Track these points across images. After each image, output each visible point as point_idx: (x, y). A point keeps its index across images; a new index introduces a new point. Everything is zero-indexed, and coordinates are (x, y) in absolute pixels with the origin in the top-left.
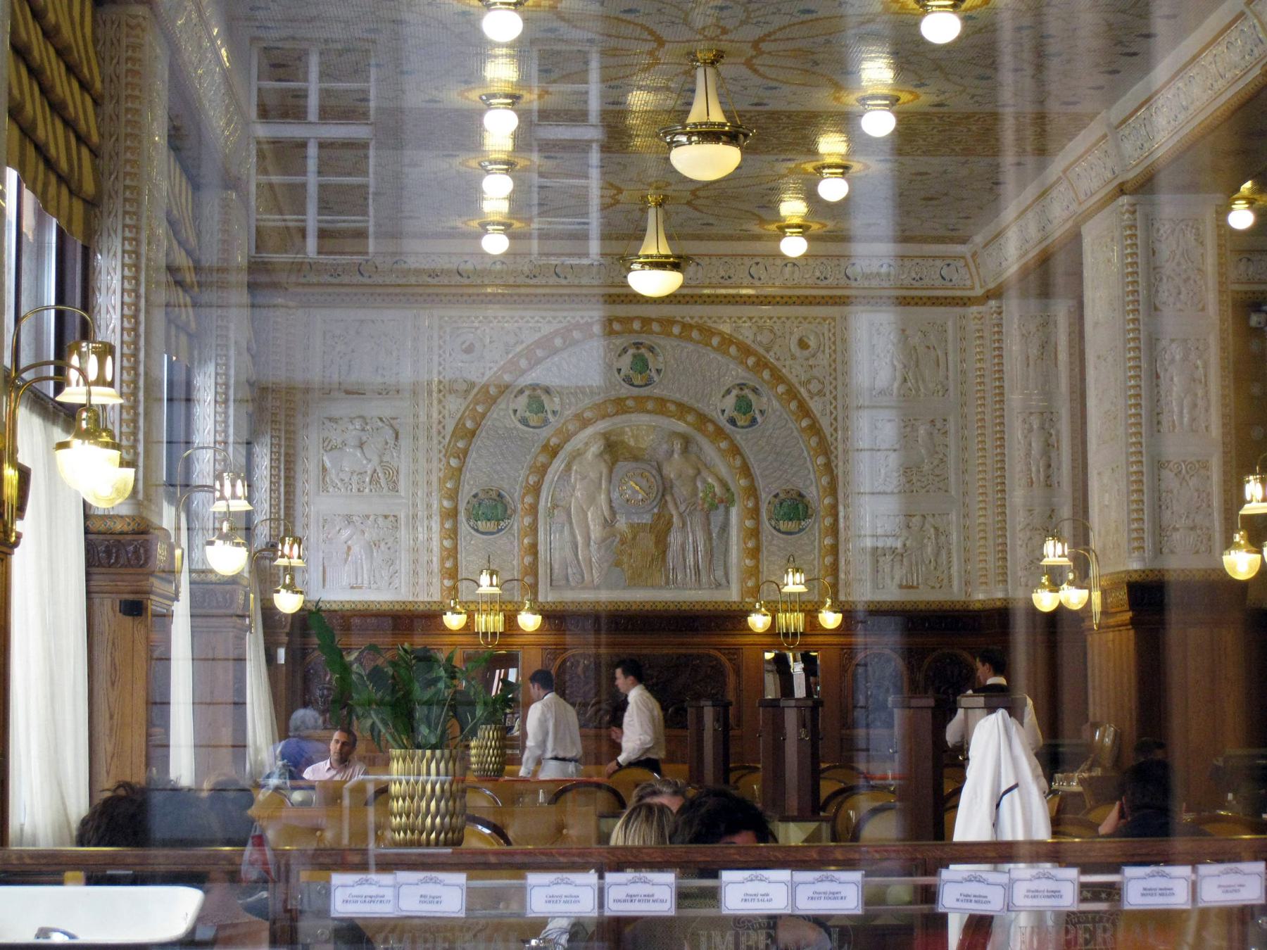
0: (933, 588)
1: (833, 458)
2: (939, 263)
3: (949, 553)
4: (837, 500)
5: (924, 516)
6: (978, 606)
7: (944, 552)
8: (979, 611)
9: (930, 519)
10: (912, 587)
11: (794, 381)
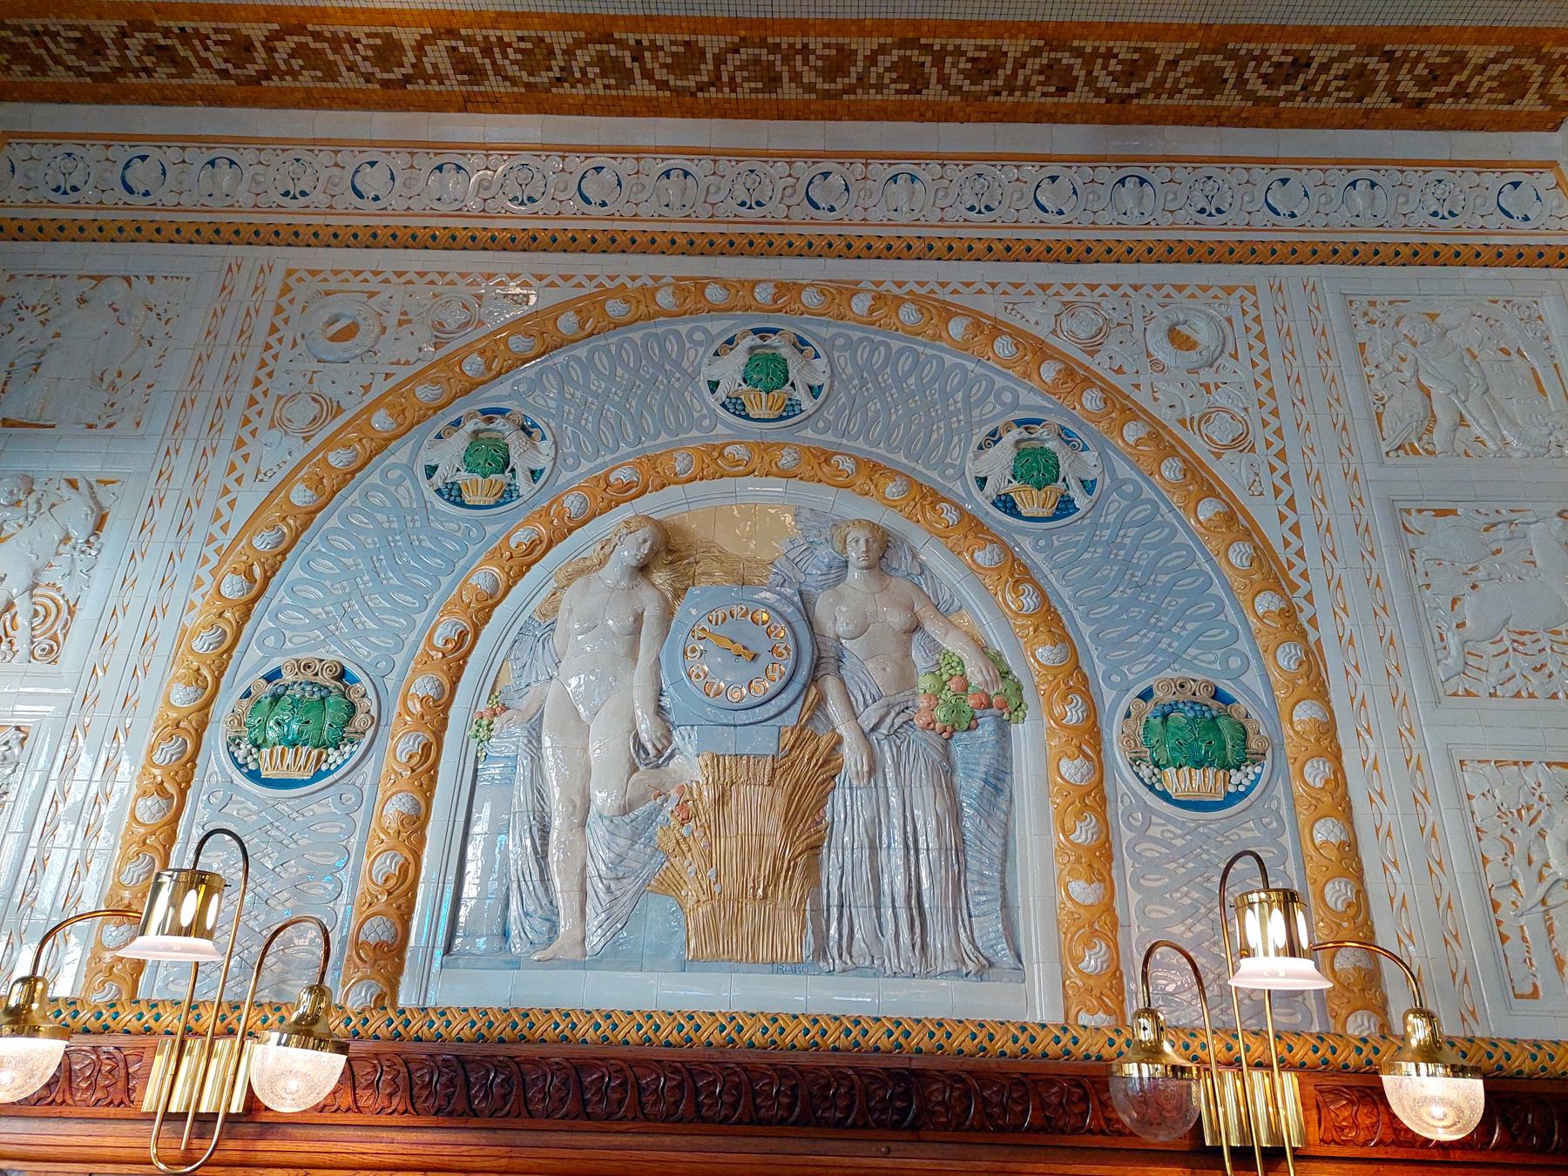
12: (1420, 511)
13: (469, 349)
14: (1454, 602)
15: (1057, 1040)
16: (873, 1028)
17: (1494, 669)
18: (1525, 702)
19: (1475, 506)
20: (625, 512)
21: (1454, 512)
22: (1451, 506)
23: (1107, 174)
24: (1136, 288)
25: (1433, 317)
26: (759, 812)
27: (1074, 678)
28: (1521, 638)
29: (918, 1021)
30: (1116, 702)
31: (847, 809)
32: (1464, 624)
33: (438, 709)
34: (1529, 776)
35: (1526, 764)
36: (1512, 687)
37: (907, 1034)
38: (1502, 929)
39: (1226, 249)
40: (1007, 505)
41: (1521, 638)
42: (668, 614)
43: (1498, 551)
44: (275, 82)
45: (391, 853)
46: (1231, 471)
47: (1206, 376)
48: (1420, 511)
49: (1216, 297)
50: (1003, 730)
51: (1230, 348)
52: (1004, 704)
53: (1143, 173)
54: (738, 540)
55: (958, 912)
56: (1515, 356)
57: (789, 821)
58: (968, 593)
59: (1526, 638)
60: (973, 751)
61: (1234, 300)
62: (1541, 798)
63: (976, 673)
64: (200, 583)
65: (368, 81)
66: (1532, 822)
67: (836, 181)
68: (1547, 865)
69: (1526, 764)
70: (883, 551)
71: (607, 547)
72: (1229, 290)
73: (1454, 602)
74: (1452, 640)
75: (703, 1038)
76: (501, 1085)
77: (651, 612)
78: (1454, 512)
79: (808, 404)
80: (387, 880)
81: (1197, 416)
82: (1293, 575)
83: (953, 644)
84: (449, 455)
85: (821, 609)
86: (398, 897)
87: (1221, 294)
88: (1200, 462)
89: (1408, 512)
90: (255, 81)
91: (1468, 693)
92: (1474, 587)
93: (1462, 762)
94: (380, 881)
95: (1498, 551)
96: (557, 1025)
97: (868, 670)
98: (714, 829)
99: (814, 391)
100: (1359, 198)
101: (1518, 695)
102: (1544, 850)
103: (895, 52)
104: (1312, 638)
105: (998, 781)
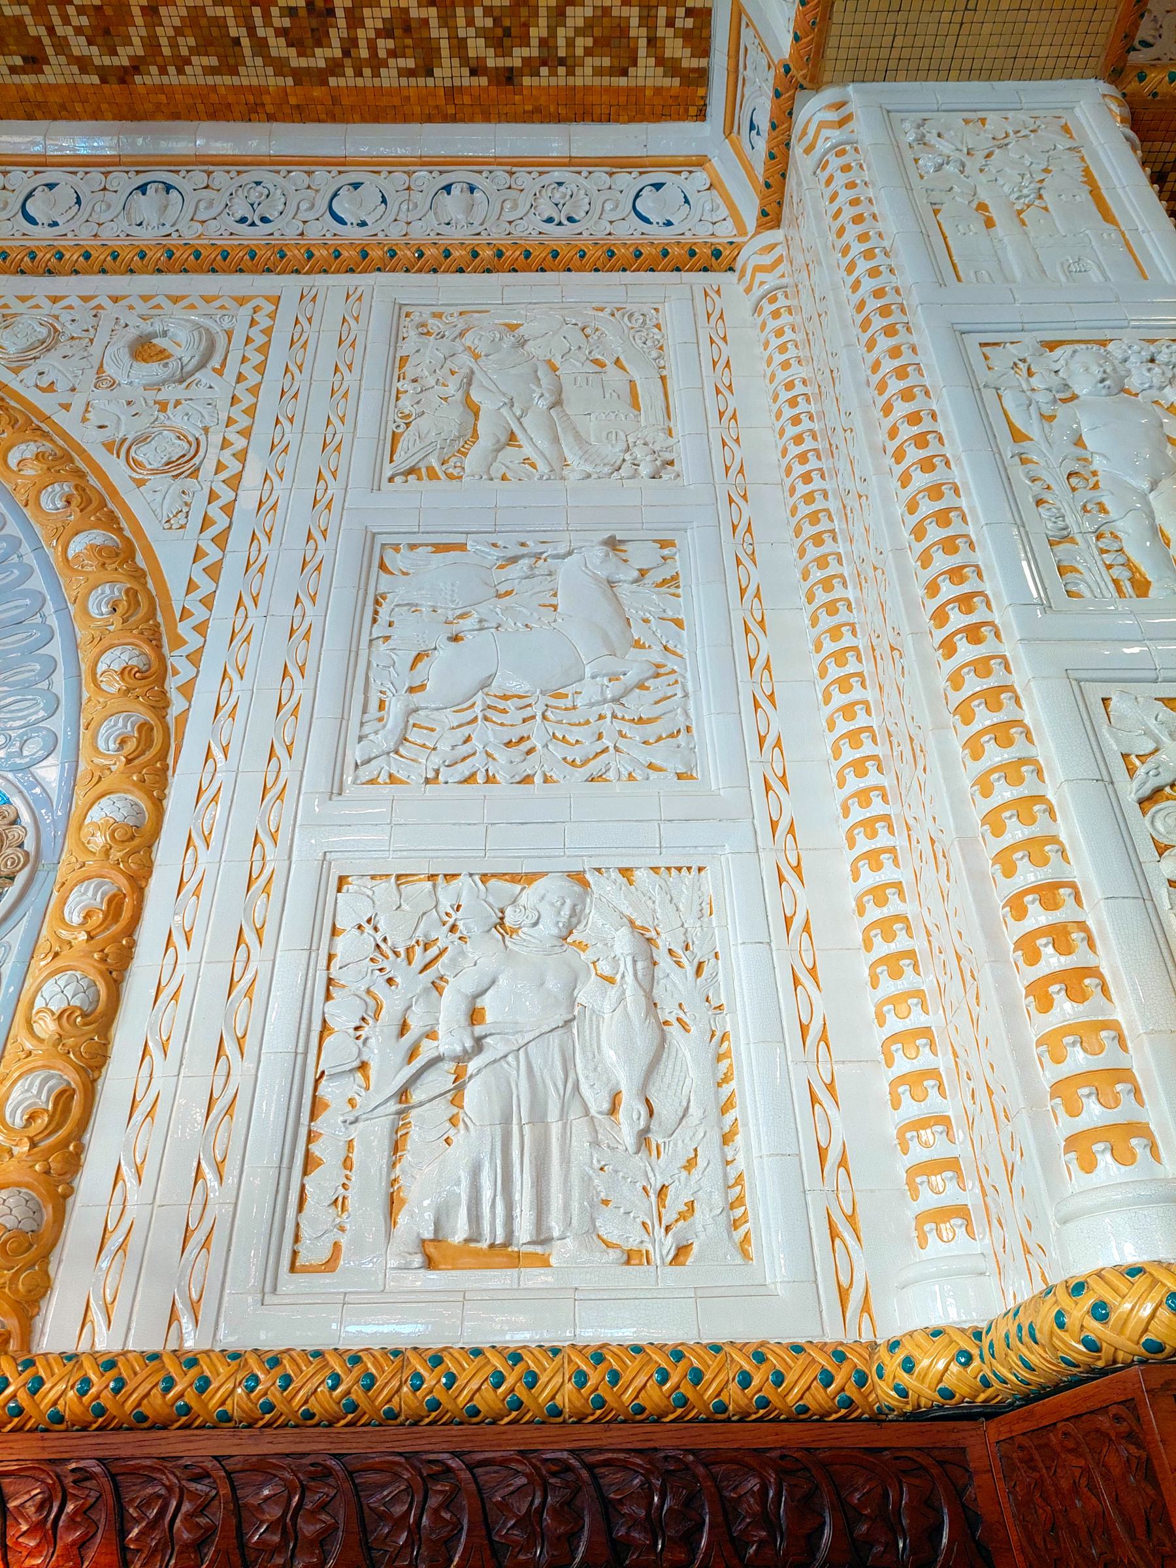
0: (630, 1258)
1: (177, 660)
2: (627, 181)
3: (719, 1047)
4: (158, 804)
5: (579, 878)
6: (936, 1374)
7: (687, 1050)
8: (953, 1414)
9: (605, 887)
10: (503, 1254)
11: (89, 438)
12: (412, 547)
14: (418, 658)
15: (745, 1380)
16: (712, 1364)
17: (444, 747)
18: (479, 788)
19: (492, 538)
21: (462, 547)
22: (460, 539)
23: (123, 181)
24: (115, 299)
25: (512, 328)
28: (501, 704)
29: (717, 1348)
32: (422, 687)
34: (446, 895)
35: (450, 877)
36: (464, 769)
37: (532, 1380)
38: (315, 1149)
39: (684, 252)
41: (501, 704)
43: (508, 593)
44: (152, 77)
45: (43, 1074)
47: (170, 393)
48: (412, 547)
49: (222, 307)
51: (215, 362)
53: (475, 179)
56: (611, 368)
59: (510, 705)
61: (246, 311)
62: (453, 928)
65: (474, 72)
66: (426, 967)
68: (431, 1035)
69: (450, 877)
72: (241, 301)
73: (418, 658)
74: (395, 708)
75: (462, 1400)
76: (73, 1523)
78: (462, 547)
80: (32, 1118)
81: (130, 438)
82: (184, 629)
86: (51, 1150)
87: (229, 303)
88: (114, 493)
89: (396, 548)
90: (124, 76)
91: (392, 779)
92: (455, 639)
93: (342, 880)
94: (19, 1122)
95: (508, 593)
96: (170, 1383)
100: (452, 205)
101: (470, 779)
102: (434, 1011)
103: (518, 63)
104: (174, 711)
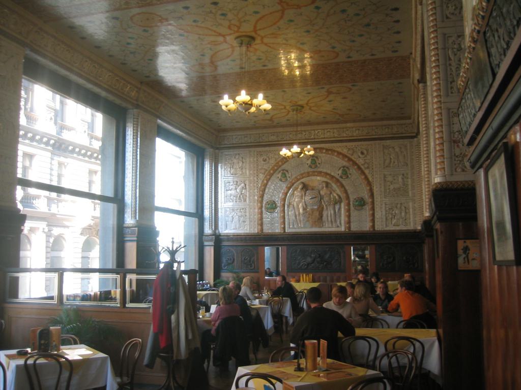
13: (279, 161)
20: (299, 182)
26: (317, 214)
27: (348, 198)
30: (352, 200)
31: (325, 213)
33: (284, 205)
40: (341, 177)
42: (305, 194)
46: (367, 172)
50: (340, 205)
52: (340, 202)
54: (315, 184)
55: (336, 221)
57: (319, 214)
58: (337, 189)
60: (337, 207)
63: (337, 197)
64: (255, 167)
67: (320, 133)
70: (327, 184)
71: (298, 186)
77: (303, 194)
79: (319, 166)
83: (335, 195)
84: (279, 175)
85: (321, 192)
97: (326, 199)
98: (312, 215)
99: (319, 164)
105: (340, 209)
